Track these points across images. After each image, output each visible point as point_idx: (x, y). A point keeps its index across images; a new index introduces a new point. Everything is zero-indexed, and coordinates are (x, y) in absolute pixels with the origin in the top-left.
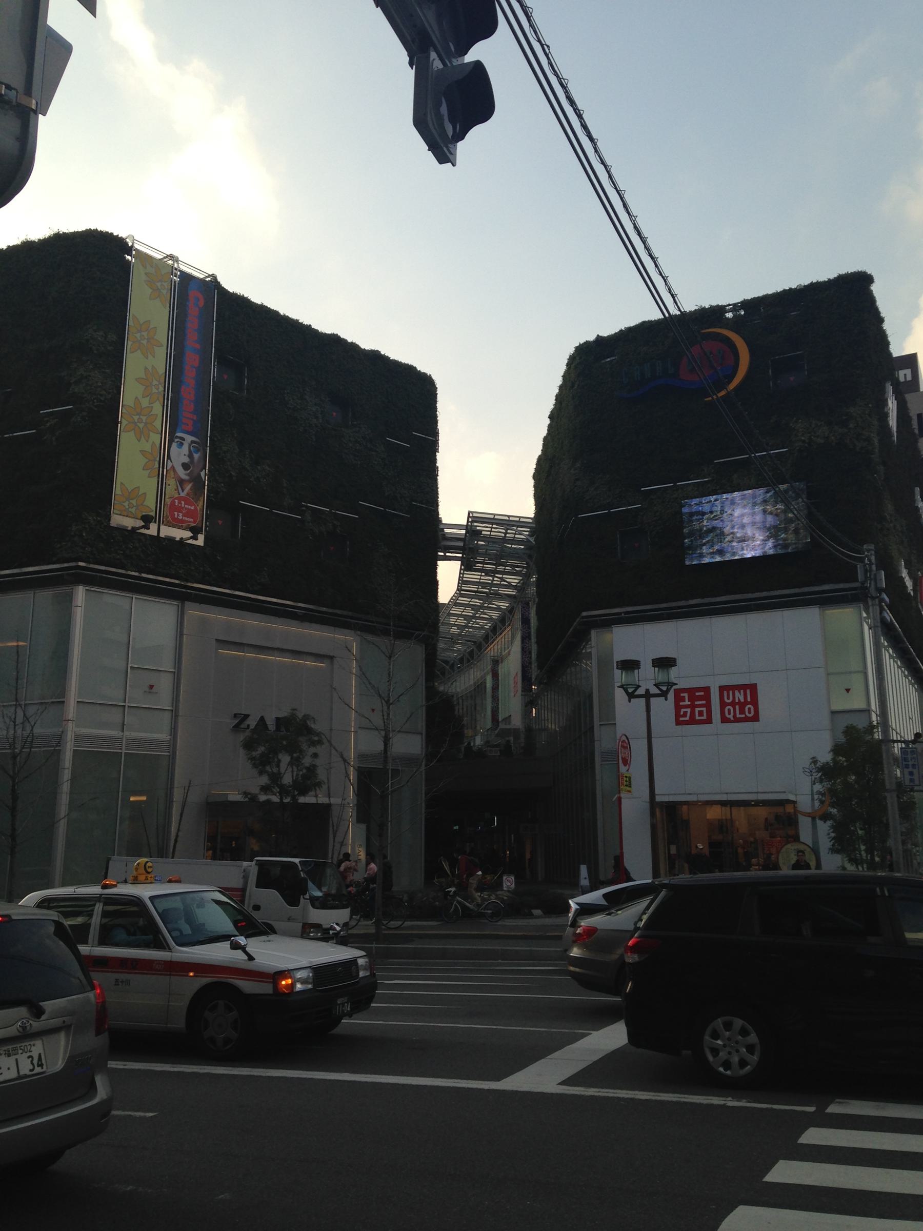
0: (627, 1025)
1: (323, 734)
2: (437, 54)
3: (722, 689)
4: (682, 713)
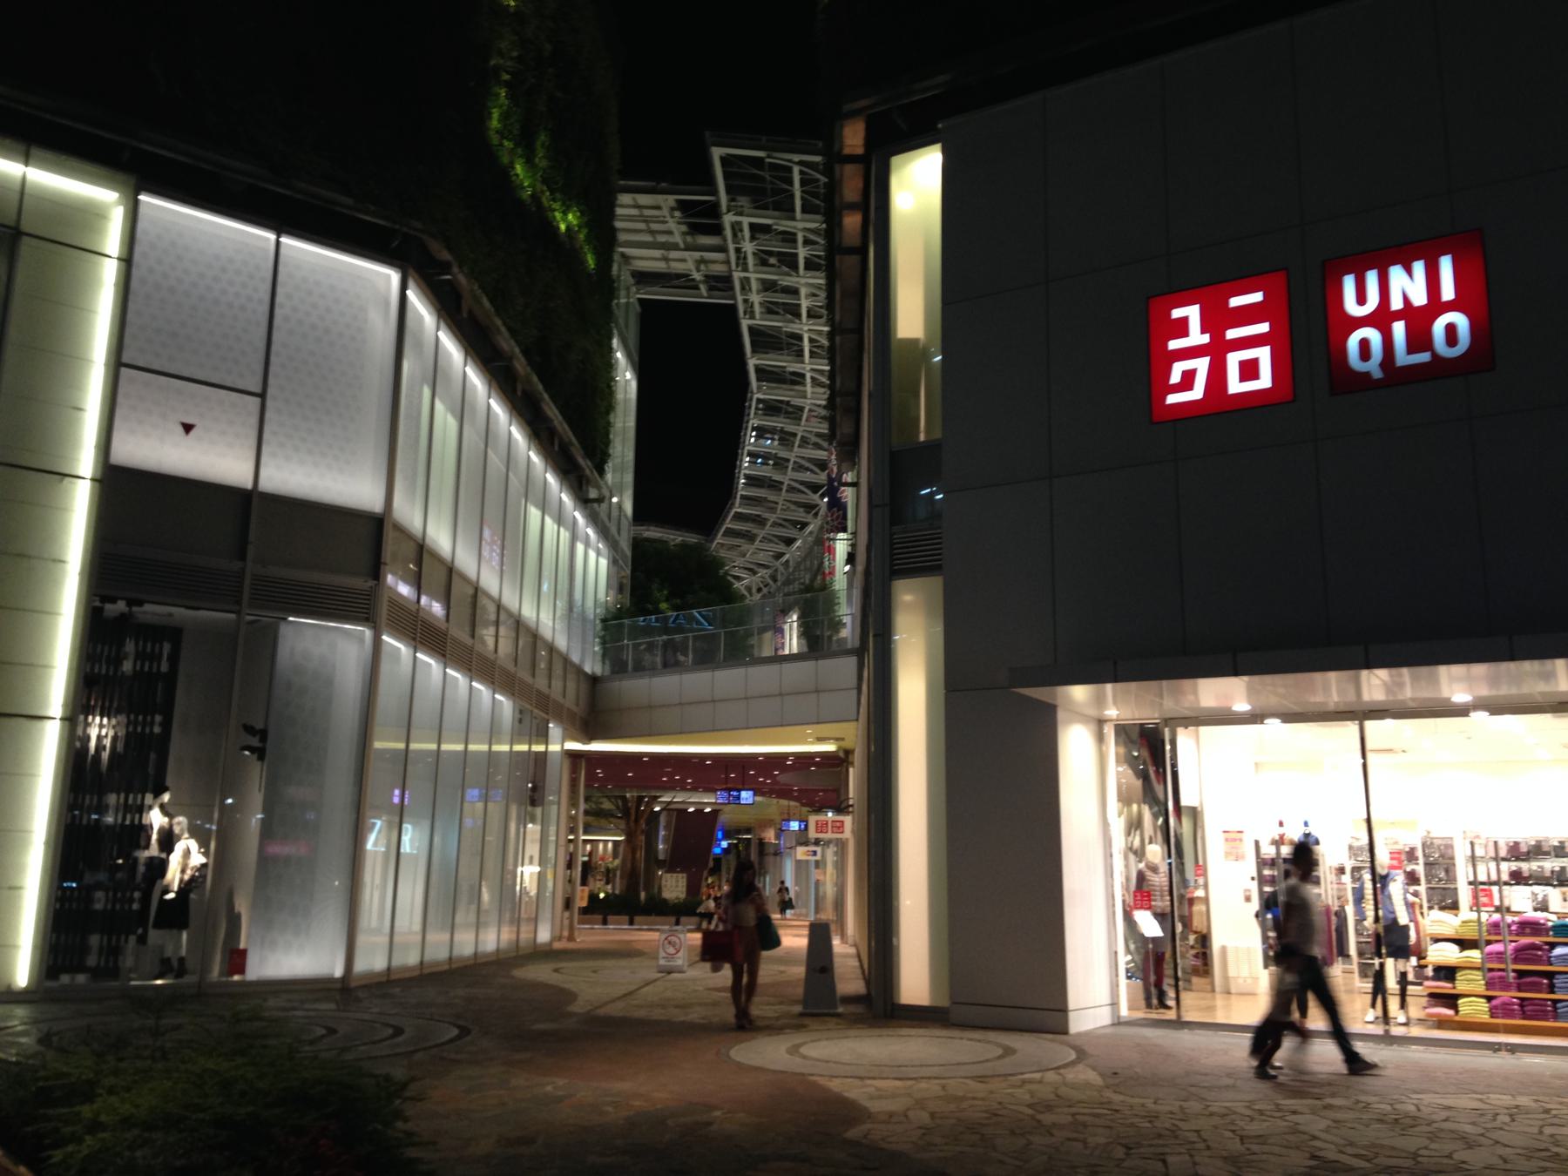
0: (944, 152)
2: (848, 163)
4: (1175, 378)
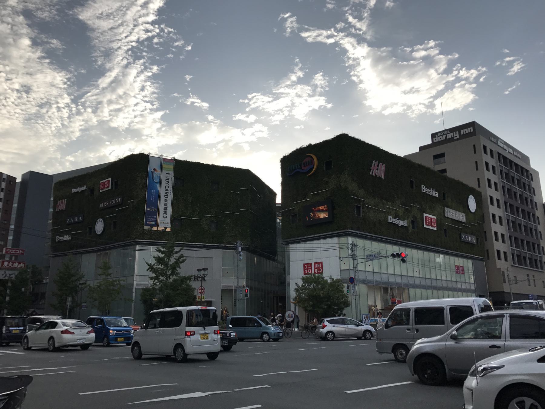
1: (272, 101)
3: (315, 263)
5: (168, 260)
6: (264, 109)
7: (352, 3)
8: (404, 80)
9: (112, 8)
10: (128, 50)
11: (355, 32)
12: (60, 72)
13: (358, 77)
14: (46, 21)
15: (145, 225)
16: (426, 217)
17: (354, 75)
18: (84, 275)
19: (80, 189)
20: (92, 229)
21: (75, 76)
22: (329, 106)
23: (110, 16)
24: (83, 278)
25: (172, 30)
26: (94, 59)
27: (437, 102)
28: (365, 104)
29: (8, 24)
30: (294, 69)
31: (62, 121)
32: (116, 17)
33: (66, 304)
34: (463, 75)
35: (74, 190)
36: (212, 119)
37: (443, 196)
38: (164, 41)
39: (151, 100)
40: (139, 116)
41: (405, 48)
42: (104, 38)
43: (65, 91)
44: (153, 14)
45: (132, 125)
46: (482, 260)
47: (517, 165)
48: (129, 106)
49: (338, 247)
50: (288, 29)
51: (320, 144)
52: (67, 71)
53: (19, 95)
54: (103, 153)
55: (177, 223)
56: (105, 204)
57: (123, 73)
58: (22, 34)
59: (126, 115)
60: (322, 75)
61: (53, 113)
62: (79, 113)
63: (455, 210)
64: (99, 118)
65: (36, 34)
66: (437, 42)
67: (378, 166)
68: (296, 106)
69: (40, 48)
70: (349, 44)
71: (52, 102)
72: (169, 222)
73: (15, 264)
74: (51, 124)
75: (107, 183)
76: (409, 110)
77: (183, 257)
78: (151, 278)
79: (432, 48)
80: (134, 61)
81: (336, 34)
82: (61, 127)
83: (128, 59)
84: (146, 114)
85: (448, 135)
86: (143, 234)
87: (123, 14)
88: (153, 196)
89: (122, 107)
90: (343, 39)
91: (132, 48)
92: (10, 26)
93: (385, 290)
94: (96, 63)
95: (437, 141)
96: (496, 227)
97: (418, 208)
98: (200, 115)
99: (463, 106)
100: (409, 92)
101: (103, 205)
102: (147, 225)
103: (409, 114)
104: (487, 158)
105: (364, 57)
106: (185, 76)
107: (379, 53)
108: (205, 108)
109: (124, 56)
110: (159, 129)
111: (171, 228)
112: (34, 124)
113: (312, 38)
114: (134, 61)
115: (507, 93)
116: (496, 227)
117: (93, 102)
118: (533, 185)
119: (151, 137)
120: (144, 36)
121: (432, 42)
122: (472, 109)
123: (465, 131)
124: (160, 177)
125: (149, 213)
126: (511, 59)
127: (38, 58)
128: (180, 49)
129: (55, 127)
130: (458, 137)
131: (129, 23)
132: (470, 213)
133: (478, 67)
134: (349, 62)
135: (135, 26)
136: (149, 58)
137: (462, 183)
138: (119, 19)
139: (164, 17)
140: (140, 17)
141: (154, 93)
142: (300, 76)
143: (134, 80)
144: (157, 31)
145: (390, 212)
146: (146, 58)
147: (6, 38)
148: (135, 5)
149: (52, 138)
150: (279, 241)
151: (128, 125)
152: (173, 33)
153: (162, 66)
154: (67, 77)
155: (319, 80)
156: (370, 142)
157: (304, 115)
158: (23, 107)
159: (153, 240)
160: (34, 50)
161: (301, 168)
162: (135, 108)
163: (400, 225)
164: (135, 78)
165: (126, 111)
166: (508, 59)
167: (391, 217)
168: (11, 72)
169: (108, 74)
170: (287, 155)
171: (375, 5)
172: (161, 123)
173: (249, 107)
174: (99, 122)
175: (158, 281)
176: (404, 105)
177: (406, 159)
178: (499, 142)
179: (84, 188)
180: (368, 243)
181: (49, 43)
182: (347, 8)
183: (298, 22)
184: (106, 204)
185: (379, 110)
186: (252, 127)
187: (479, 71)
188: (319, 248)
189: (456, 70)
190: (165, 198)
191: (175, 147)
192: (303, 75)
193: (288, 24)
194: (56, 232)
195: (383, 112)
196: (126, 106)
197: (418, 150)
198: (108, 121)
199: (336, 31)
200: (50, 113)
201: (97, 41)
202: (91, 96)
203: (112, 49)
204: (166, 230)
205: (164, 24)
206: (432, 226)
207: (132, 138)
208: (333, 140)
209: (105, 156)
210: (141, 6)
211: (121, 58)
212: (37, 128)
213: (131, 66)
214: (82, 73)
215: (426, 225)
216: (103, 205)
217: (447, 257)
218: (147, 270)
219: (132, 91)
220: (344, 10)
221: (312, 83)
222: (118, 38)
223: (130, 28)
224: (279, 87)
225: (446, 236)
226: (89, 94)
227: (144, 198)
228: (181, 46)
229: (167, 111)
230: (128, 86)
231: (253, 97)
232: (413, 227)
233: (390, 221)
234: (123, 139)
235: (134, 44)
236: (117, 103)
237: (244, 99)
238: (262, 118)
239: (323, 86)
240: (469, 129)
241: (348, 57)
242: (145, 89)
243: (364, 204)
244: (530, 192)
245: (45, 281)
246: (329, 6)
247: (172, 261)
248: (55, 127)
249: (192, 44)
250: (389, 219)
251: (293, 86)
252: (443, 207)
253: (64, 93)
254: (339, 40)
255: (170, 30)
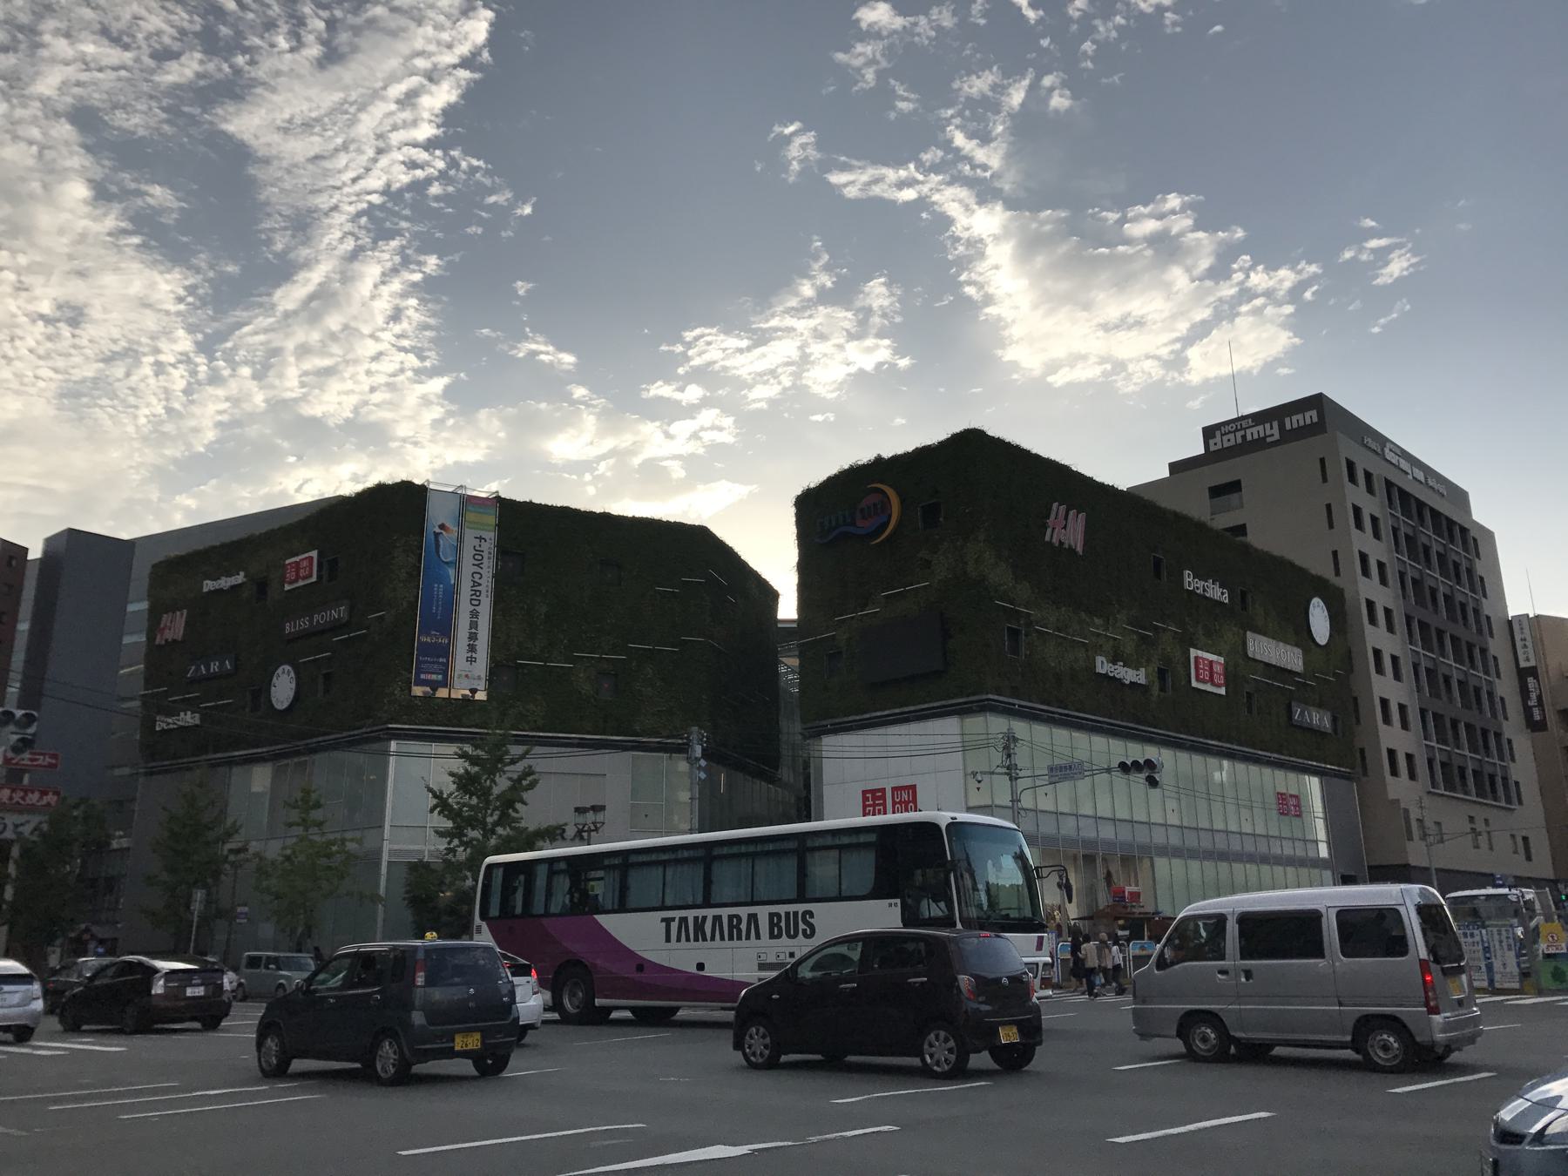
1: (749, 349)
3: (894, 789)
5: (488, 782)
6: (725, 369)
7: (962, 99)
8: (1101, 296)
9: (319, 107)
10: (359, 214)
11: (972, 173)
12: (169, 271)
13: (980, 286)
14: (135, 137)
15: (416, 685)
16: (1197, 658)
17: (970, 283)
18: (241, 826)
19: (225, 583)
20: (262, 691)
21: (209, 281)
22: (904, 363)
23: (312, 127)
24: (236, 836)
25: (481, 163)
26: (263, 237)
27: (1193, 353)
28: (1000, 358)
29: (31, 143)
30: (810, 267)
31: (167, 400)
32: (331, 129)
33: (188, 907)
34: (1259, 284)
35: (209, 585)
36: (584, 396)
37: (1242, 598)
38: (458, 191)
39: (419, 345)
40: (383, 388)
41: (1104, 213)
42: (294, 181)
43: (179, 319)
44: (431, 121)
45: (364, 410)
46: (1347, 777)
47: (1435, 514)
48: (356, 361)
49: (960, 745)
50: (795, 163)
51: (906, 455)
52: (187, 269)
53: (50, 330)
54: (281, 487)
55: (505, 678)
56: (300, 625)
57: (342, 273)
58: (66, 170)
59: (349, 385)
60: (884, 284)
61: (142, 380)
62: (215, 379)
63: (1274, 638)
64: (271, 393)
65: (107, 171)
66: (1186, 198)
67: (1066, 518)
68: (813, 363)
69: (117, 208)
70: (956, 205)
71: (141, 349)
72: (483, 676)
73: (30, 795)
74: (136, 407)
75: (305, 563)
76: (1118, 374)
77: (533, 773)
78: (440, 834)
79: (1173, 212)
80: (375, 242)
81: (920, 177)
82: (165, 417)
83: (357, 238)
84: (402, 382)
85: (1249, 432)
86: (413, 709)
87: (349, 122)
88: (438, 601)
89: (337, 364)
90: (938, 190)
91: (368, 207)
92: (34, 149)
93: (1089, 859)
94: (268, 247)
95: (1219, 446)
96: (1384, 687)
97: (1176, 632)
98: (551, 384)
99: (1260, 363)
100: (1117, 327)
101: (295, 627)
102: (420, 683)
103: (1119, 384)
104: (1357, 494)
105: (996, 238)
106: (515, 282)
107: (1034, 226)
108: (565, 367)
109: (346, 230)
110: (438, 424)
111: (490, 691)
112: (89, 407)
113: (856, 188)
114: (375, 242)
115: (1376, 330)
116: (1384, 687)
117: (257, 350)
118: (1480, 568)
119: (416, 444)
120: (403, 178)
121: (1175, 197)
122: (1285, 371)
123: (1295, 421)
124: (458, 549)
125: (426, 649)
126: (1383, 242)
127: (110, 234)
128: (503, 213)
129: (147, 416)
130: (1277, 437)
131: (365, 143)
132: (1313, 647)
133: (1298, 264)
134: (956, 249)
135: (380, 151)
136: (415, 235)
137: (1292, 565)
138: (336, 135)
139: (459, 129)
140: (395, 128)
141: (425, 327)
142: (823, 286)
143: (371, 292)
144: (441, 165)
145: (1101, 646)
146: (407, 235)
147: (23, 180)
148: (384, 99)
149: (136, 445)
150: (791, 728)
151: (351, 412)
152: (482, 172)
153: (451, 258)
154: (187, 283)
155: (878, 296)
156: (1044, 453)
157: (834, 386)
158: (60, 363)
159: (438, 725)
160: (98, 212)
161: (853, 524)
162: (374, 366)
163: (1127, 682)
164: (376, 286)
165: (347, 375)
166: (1374, 243)
167: (1104, 659)
168: (31, 269)
169: (302, 276)
170: (812, 486)
171: (1023, 105)
172: (442, 406)
173: (686, 365)
174: (272, 402)
175: (461, 841)
176: (1103, 360)
177: (1142, 499)
178: (1387, 450)
179: (240, 578)
180: (1041, 731)
181: (140, 193)
182: (950, 112)
183: (819, 145)
184: (303, 624)
185: (1037, 373)
186: (694, 418)
187: (1300, 272)
188: (933, 747)
189: (1241, 269)
190: (473, 608)
191: (479, 469)
192: (833, 283)
193: (794, 151)
194: (154, 706)
195: (1050, 379)
196: (347, 362)
197: (1166, 473)
198: (296, 400)
199: (921, 170)
200: (134, 378)
201: (276, 190)
202: (253, 334)
203: (315, 211)
204: (473, 697)
205: (460, 148)
206: (1213, 684)
207: (361, 447)
208: (943, 445)
209: (283, 493)
210: (398, 102)
211: (338, 234)
212: (96, 420)
213: (366, 256)
214: (229, 272)
215: (1198, 680)
216: (295, 627)
217: (1241, 767)
218: (432, 811)
219: (365, 322)
220: (943, 116)
221: (858, 304)
222: (331, 182)
223: (366, 158)
224: (768, 312)
225: (1250, 711)
226: (246, 329)
227: (413, 606)
228: (506, 204)
229: (462, 375)
230: (354, 309)
231: (697, 339)
232: (1162, 689)
233: (1099, 670)
234: (335, 448)
235: (376, 199)
236: (323, 351)
237: (674, 344)
238: (720, 392)
239: (888, 311)
240: (1307, 415)
241: (952, 236)
242: (403, 318)
243: (1029, 624)
244: (1473, 590)
245: (115, 845)
246: (902, 105)
247: (502, 784)
248: (147, 416)
249: (535, 199)
250: (1098, 664)
251: (804, 309)
252: (1241, 632)
253: (176, 325)
254: (929, 194)
255: (475, 162)
